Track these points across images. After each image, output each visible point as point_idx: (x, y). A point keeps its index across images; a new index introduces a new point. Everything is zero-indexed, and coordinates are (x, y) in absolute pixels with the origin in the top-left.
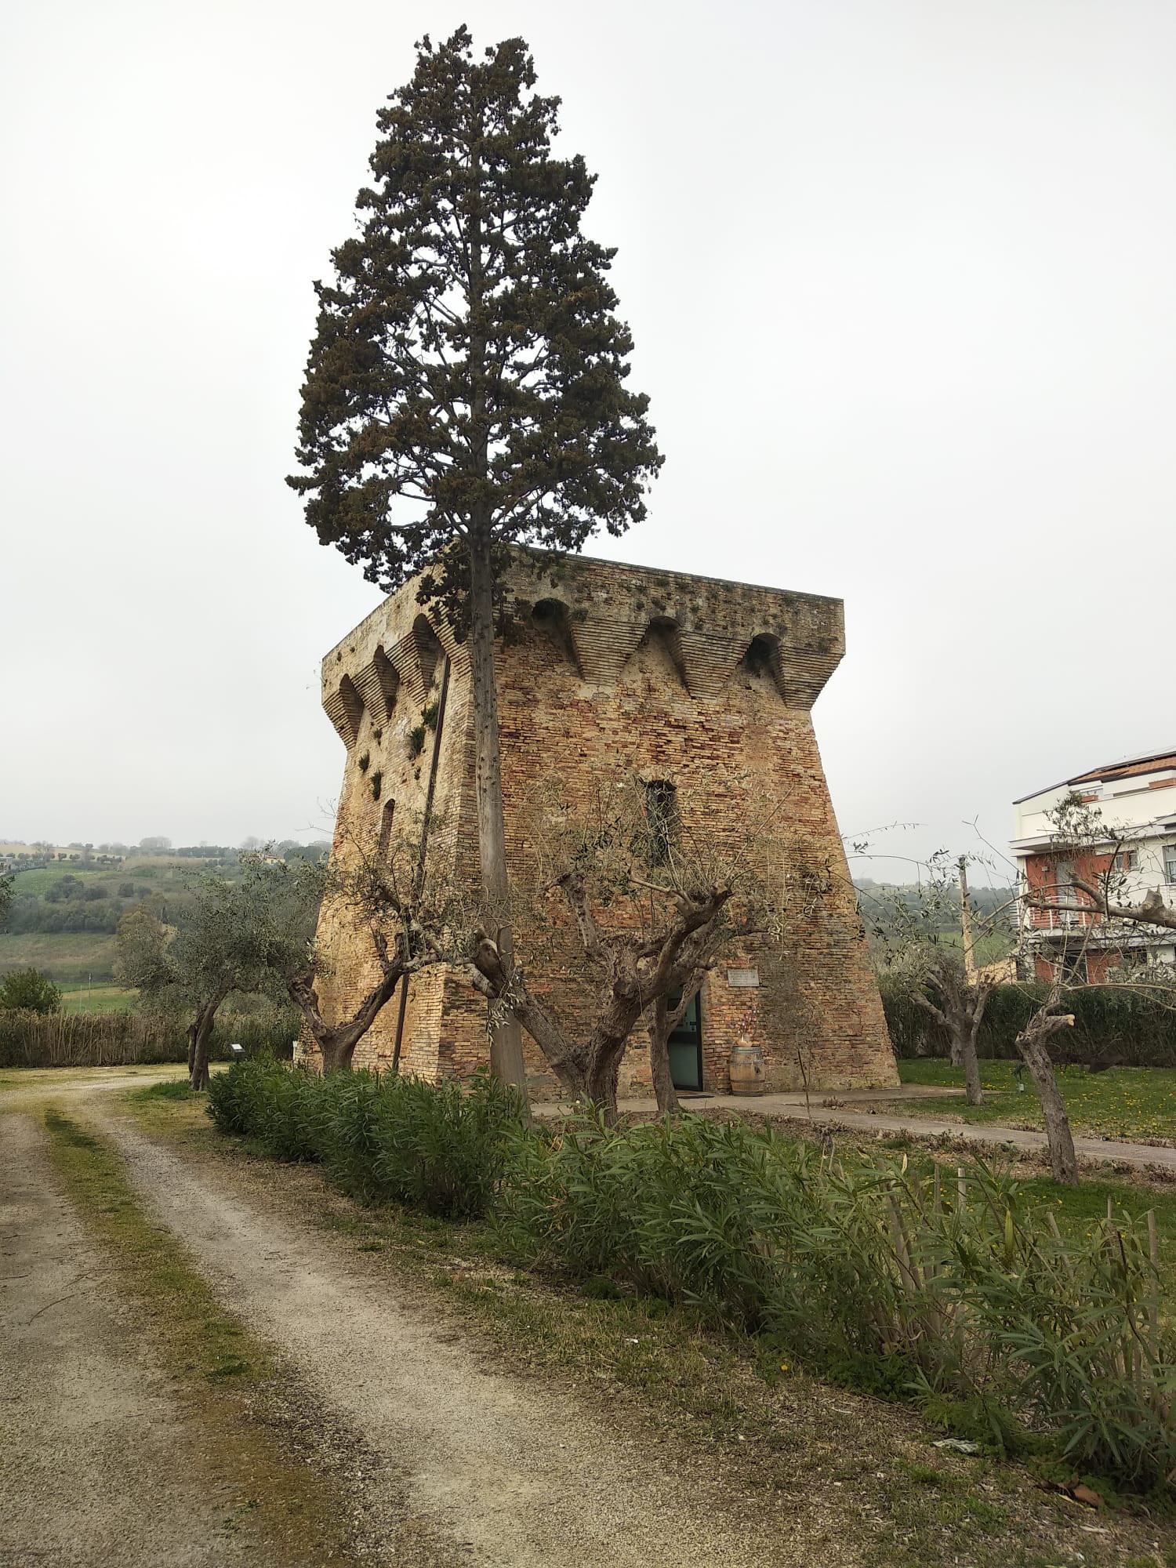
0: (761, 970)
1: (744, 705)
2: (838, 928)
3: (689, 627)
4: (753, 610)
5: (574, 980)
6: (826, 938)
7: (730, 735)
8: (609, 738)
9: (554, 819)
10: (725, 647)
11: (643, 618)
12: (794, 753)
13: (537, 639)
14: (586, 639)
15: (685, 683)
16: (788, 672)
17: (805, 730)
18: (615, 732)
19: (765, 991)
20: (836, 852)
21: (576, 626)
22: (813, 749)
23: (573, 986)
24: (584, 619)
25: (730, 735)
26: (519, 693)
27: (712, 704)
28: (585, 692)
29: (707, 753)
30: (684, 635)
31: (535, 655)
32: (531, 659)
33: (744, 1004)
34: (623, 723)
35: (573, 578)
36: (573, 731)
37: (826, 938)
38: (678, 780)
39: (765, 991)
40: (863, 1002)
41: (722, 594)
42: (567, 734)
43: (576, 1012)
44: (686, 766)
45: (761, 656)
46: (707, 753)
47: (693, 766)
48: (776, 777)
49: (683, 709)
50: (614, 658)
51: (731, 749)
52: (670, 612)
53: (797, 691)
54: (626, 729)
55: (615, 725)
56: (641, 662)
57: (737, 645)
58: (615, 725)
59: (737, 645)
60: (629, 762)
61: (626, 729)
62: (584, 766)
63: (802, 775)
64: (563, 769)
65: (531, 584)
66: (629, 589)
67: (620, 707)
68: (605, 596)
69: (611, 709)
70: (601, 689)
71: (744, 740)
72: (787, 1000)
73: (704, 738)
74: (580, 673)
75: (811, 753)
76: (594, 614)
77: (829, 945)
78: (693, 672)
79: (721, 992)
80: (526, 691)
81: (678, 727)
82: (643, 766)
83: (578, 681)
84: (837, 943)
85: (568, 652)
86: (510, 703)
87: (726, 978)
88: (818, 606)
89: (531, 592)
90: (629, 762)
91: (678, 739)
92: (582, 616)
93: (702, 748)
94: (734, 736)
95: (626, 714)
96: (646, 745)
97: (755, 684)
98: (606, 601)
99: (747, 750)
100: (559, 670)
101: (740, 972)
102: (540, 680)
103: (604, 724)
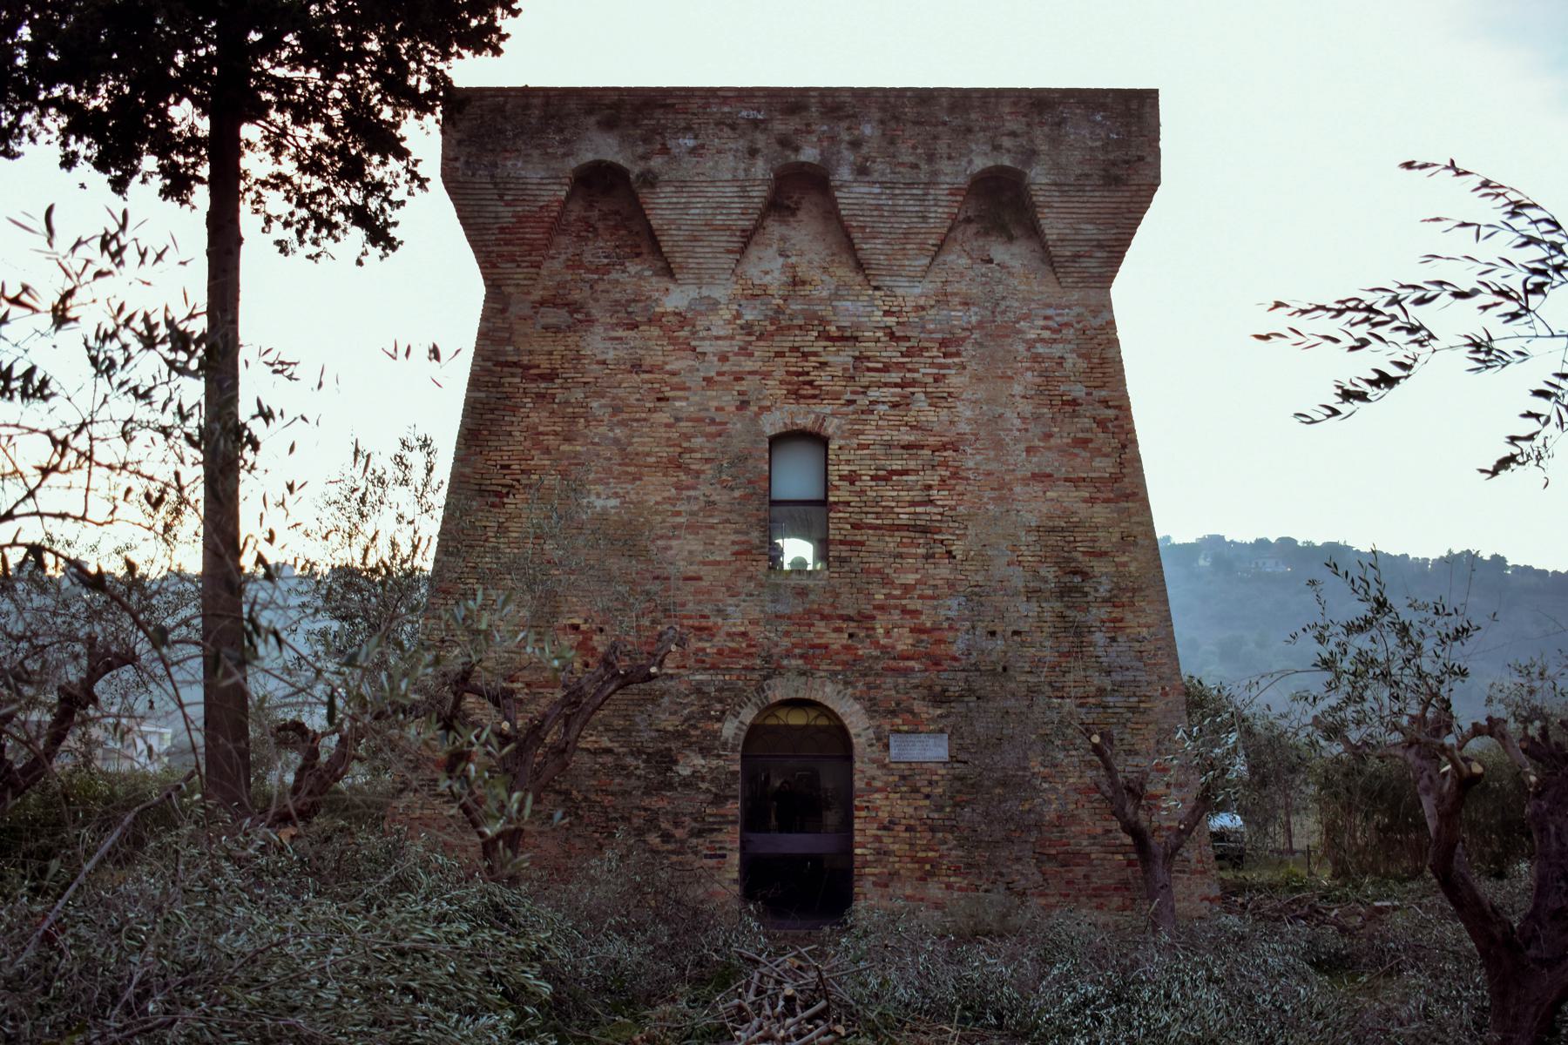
0: (955, 733)
1: (976, 291)
2: (1125, 661)
3: (844, 174)
4: (969, 130)
5: (608, 751)
6: (1097, 680)
7: (943, 343)
8: (712, 367)
9: (599, 503)
10: (921, 199)
11: (760, 169)
12: (1068, 365)
13: (600, 225)
14: (662, 208)
15: (860, 266)
16: (1053, 226)
17: (1097, 322)
18: (723, 358)
19: (960, 769)
20: (1137, 530)
21: (644, 194)
22: (1110, 354)
23: (609, 760)
24: (653, 185)
25: (943, 343)
26: (564, 312)
27: (911, 293)
28: (676, 299)
29: (895, 377)
30: (839, 188)
31: (596, 251)
32: (587, 257)
33: (915, 790)
34: (740, 340)
35: (635, 123)
36: (648, 362)
37: (1097, 680)
38: (831, 427)
39: (960, 769)
40: (1161, 789)
41: (910, 112)
42: (637, 367)
43: (607, 800)
44: (851, 402)
45: (1001, 204)
46: (895, 377)
47: (863, 401)
48: (1027, 408)
49: (859, 309)
50: (722, 240)
51: (942, 366)
52: (809, 154)
53: (1076, 257)
54: (745, 351)
55: (724, 345)
56: (783, 239)
57: (941, 192)
58: (724, 345)
59: (941, 192)
60: (743, 405)
61: (745, 351)
62: (663, 417)
63: (1091, 410)
64: (623, 423)
65: (565, 142)
66: (733, 127)
67: (738, 316)
68: (691, 143)
69: (719, 323)
70: (705, 292)
71: (968, 350)
72: (1004, 784)
73: (892, 353)
74: (668, 272)
75: (1104, 361)
76: (673, 175)
77: (1101, 691)
78: (871, 249)
79: (872, 770)
80: (574, 307)
81: (842, 338)
82: (768, 409)
83: (665, 282)
84: (1118, 688)
85: (646, 242)
86: (546, 328)
87: (887, 747)
88: (1103, 107)
89: (565, 155)
90: (743, 405)
91: (841, 358)
92: (650, 180)
93: (886, 369)
94: (950, 345)
95: (748, 328)
96: (780, 373)
97: (1000, 251)
98: (693, 151)
99: (972, 366)
100: (633, 268)
101: (913, 737)
102: (600, 287)
103: (705, 346)
